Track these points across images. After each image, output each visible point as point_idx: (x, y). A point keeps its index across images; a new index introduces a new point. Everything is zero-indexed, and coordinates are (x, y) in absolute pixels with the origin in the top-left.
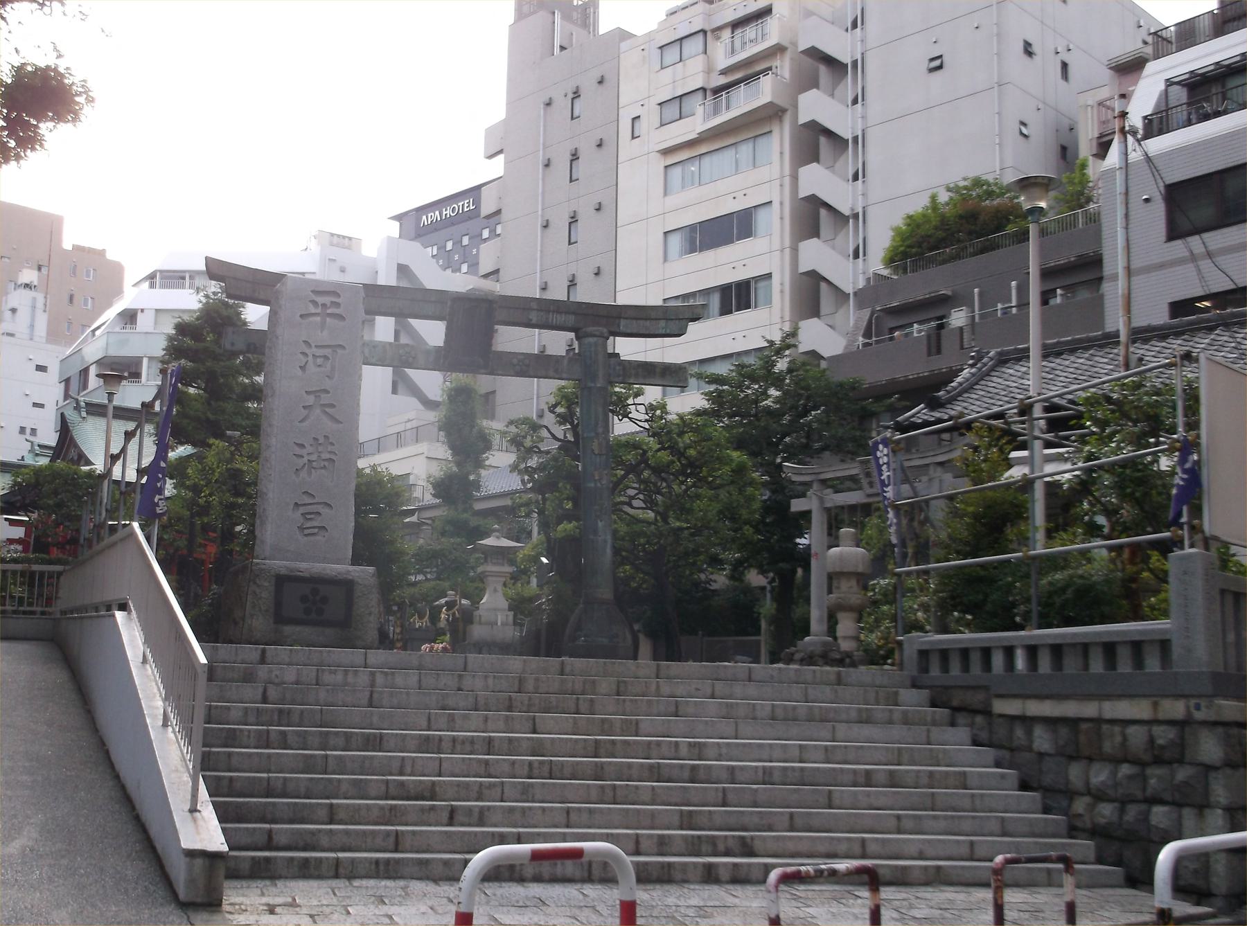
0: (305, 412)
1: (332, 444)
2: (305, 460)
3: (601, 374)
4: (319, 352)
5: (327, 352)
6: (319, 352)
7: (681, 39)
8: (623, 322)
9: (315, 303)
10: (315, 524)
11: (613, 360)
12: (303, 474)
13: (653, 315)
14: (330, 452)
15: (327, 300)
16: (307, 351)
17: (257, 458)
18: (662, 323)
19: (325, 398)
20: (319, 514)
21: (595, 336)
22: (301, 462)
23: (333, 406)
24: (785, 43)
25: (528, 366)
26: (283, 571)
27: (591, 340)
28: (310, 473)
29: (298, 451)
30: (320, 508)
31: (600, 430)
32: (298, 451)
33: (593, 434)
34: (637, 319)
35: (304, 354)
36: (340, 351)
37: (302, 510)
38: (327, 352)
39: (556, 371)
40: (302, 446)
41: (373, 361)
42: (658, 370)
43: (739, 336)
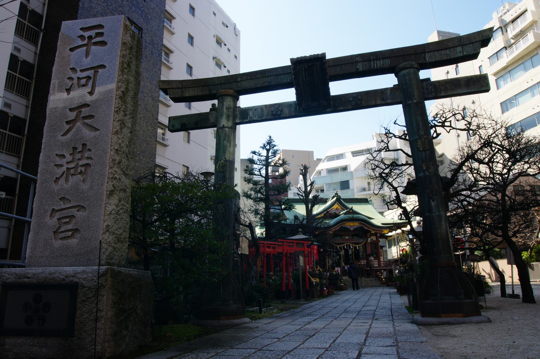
0: (67, 127)
1: (90, 150)
2: (64, 169)
3: (416, 93)
4: (85, 74)
5: (90, 73)
6: (85, 74)
7: (496, 53)
8: (427, 55)
9: (82, 37)
10: (70, 227)
11: (425, 84)
12: (62, 181)
13: (450, 45)
14: (88, 158)
15: (92, 33)
16: (73, 76)
17: (83, 181)
18: (459, 49)
19: (85, 111)
20: (73, 216)
21: (406, 68)
22: (60, 171)
23: (91, 117)
24: (536, 19)
25: (361, 100)
26: (12, 279)
27: (405, 72)
28: (67, 180)
29: (59, 161)
30: (74, 211)
31: (422, 133)
32: (59, 161)
33: (417, 137)
34: (438, 51)
35: (71, 79)
36: (100, 71)
37: (58, 215)
38: (90, 73)
39: (382, 99)
40: (63, 156)
41: (256, 118)
42: (462, 83)
43: (530, 81)
